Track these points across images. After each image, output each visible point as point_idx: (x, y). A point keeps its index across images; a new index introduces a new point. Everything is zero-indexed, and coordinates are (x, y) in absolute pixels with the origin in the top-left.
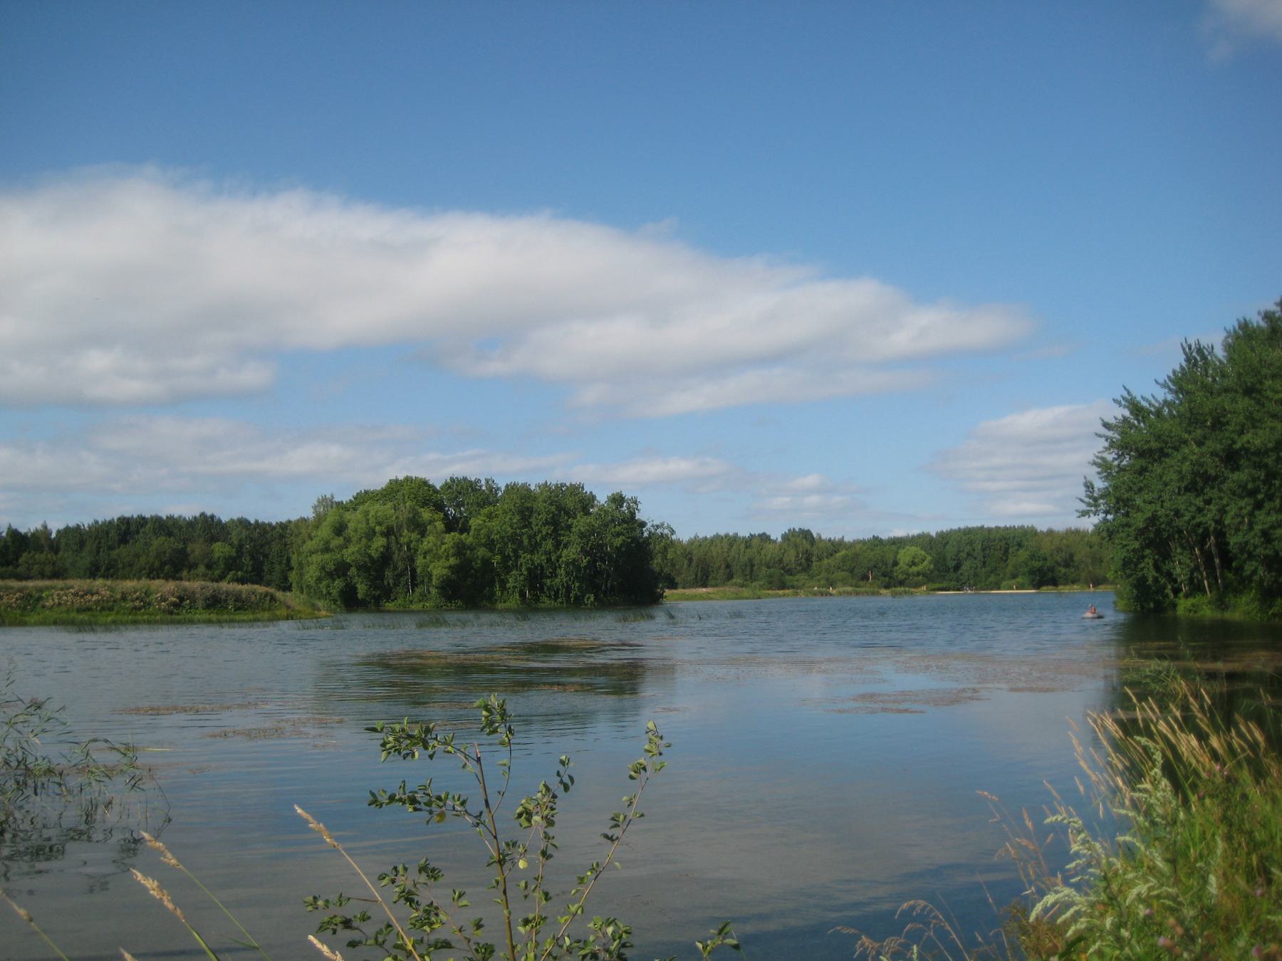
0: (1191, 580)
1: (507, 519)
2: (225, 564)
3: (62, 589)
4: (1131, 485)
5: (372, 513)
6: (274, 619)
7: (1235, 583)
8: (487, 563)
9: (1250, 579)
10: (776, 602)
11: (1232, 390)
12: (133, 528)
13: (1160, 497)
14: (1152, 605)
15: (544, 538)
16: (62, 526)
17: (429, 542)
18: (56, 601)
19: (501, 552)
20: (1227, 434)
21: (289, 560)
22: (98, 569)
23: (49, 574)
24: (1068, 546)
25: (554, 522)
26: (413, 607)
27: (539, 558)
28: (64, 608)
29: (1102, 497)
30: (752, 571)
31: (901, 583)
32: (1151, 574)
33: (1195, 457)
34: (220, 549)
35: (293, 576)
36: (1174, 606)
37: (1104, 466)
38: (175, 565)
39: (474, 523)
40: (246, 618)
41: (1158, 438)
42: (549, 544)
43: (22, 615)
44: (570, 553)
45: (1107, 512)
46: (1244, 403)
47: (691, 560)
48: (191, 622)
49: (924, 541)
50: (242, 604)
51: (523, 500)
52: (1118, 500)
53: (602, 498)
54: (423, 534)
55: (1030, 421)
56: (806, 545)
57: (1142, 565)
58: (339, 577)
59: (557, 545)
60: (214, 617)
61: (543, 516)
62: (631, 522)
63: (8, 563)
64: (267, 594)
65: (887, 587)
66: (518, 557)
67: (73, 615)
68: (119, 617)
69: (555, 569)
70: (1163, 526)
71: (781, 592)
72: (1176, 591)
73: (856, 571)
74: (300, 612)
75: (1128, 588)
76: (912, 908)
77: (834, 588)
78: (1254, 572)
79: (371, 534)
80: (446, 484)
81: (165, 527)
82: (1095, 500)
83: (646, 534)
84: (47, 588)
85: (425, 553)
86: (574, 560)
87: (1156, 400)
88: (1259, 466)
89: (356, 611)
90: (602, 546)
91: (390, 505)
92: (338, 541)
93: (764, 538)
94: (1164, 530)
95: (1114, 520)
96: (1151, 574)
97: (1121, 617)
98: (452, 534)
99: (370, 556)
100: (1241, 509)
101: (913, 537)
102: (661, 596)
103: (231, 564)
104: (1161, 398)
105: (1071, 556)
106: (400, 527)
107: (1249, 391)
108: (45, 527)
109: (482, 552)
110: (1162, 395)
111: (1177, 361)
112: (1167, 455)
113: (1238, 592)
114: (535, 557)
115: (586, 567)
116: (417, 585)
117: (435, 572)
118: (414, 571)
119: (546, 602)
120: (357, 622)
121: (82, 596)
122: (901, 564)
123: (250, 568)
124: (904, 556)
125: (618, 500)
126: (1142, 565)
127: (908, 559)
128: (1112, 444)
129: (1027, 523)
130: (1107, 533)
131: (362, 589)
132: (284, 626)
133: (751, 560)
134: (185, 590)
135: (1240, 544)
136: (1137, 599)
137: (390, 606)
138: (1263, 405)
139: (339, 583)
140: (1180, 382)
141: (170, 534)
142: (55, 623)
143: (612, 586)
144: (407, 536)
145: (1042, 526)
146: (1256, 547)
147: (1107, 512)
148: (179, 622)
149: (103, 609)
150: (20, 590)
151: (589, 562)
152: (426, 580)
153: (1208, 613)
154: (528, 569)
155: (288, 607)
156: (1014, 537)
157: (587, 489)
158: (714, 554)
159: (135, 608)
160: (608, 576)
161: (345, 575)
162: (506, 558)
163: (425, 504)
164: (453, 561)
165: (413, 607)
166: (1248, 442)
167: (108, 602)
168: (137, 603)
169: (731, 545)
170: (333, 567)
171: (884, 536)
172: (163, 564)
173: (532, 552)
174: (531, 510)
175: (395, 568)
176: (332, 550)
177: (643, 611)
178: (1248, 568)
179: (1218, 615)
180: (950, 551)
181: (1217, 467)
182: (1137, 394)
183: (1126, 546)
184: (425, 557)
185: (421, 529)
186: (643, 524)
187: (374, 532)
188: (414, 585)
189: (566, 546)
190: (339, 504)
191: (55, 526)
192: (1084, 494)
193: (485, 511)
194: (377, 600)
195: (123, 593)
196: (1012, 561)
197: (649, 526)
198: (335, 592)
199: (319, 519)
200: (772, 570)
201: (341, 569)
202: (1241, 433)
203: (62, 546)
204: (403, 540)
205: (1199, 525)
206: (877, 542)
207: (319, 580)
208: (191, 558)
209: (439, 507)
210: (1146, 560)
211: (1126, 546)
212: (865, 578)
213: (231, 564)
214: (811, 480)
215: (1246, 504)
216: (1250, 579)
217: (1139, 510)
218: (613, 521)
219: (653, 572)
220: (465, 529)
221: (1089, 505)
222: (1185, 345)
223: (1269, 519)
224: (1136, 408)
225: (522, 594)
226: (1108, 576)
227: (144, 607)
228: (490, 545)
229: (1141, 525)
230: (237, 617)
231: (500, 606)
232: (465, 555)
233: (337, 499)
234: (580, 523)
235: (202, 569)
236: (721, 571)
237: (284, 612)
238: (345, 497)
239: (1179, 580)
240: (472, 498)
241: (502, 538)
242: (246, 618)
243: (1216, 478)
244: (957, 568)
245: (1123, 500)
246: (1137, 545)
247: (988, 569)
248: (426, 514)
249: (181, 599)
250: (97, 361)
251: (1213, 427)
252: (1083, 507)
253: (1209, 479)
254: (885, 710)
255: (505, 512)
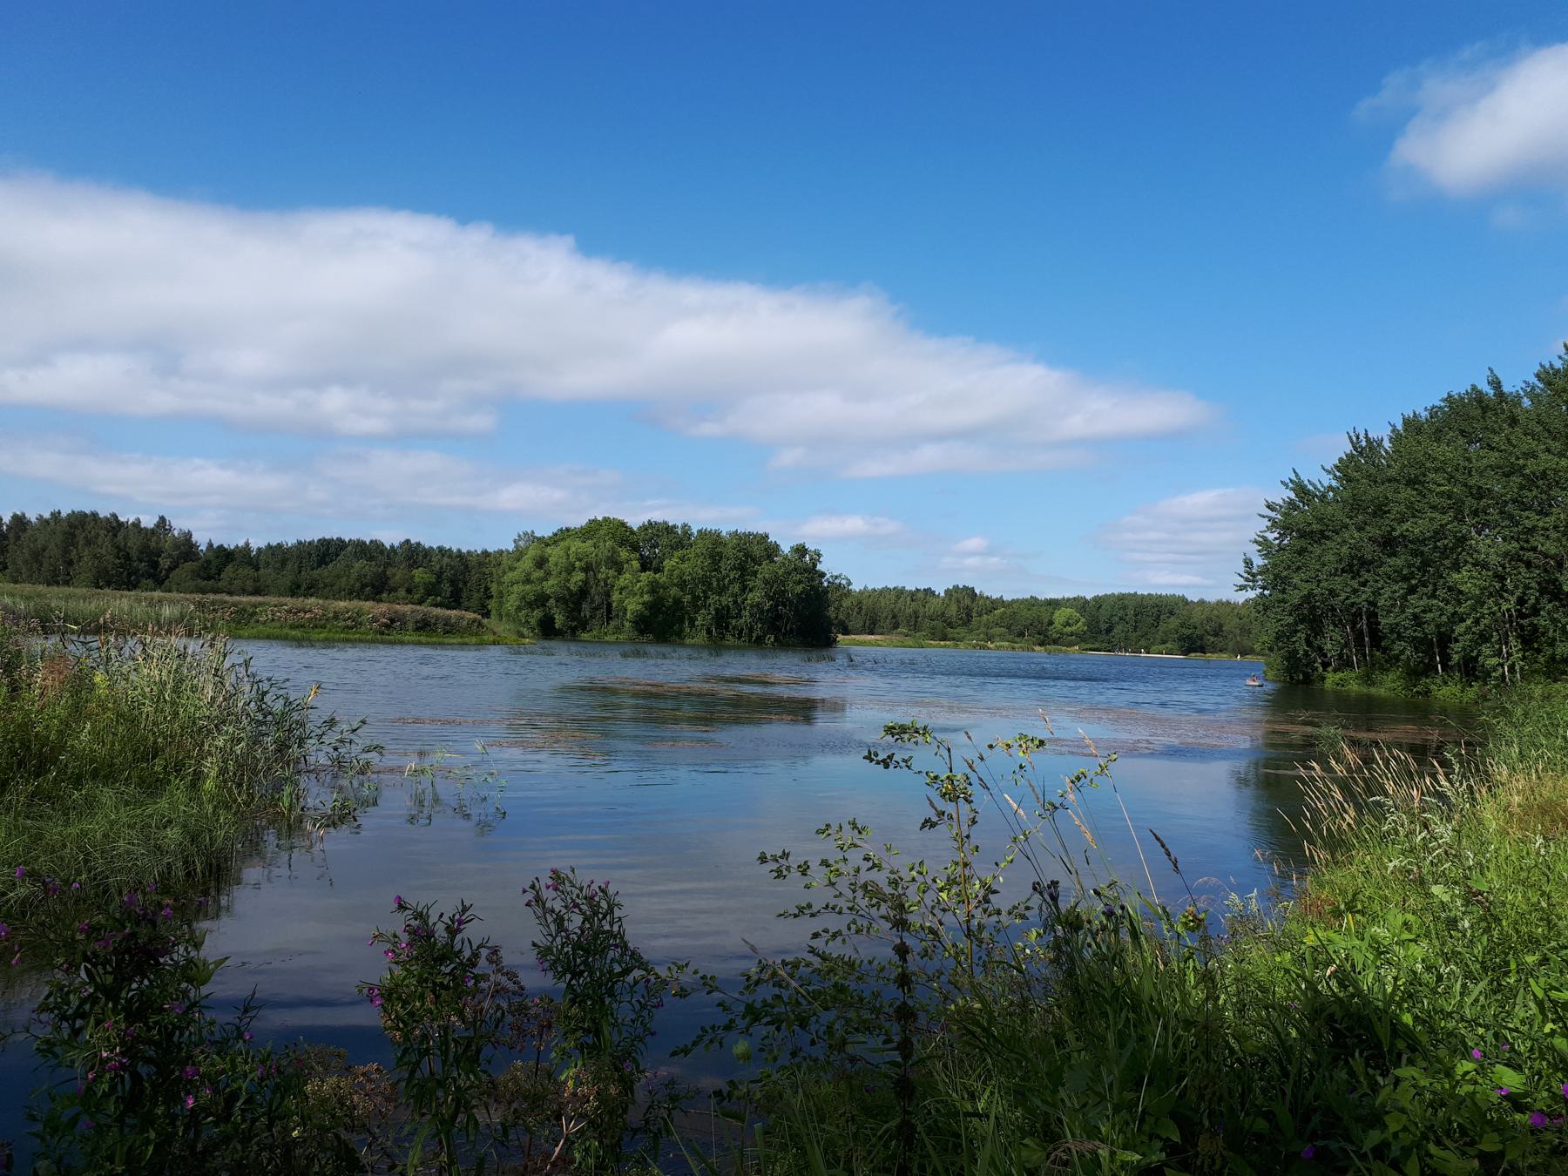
0: (1340, 656)
1: (699, 563)
2: (425, 589)
3: (275, 606)
4: (1289, 563)
5: (573, 549)
6: (481, 644)
7: (1383, 661)
8: (678, 601)
9: (1397, 658)
10: (938, 652)
11: (1395, 480)
12: (332, 550)
13: (1317, 576)
14: (1301, 677)
15: (731, 582)
16: (263, 545)
17: (625, 579)
18: (270, 616)
19: (692, 593)
20: (1387, 522)
21: (487, 589)
22: (299, 587)
23: (251, 589)
24: (1218, 617)
25: (742, 568)
26: (607, 638)
27: (726, 600)
28: (277, 624)
29: (1260, 573)
30: (916, 621)
31: (1055, 642)
32: (1302, 648)
33: (1353, 541)
34: (419, 574)
35: (492, 604)
36: (1323, 679)
37: (1263, 543)
38: (377, 588)
39: (668, 564)
40: (454, 641)
41: (1320, 520)
42: (736, 588)
43: (236, 629)
44: (755, 597)
45: (1264, 588)
46: (1406, 493)
47: (860, 608)
48: (402, 643)
49: (1080, 604)
50: (450, 629)
51: (714, 544)
52: (1276, 576)
53: (786, 548)
54: (620, 571)
55: (1200, 500)
56: (968, 601)
57: (1294, 639)
58: (538, 607)
59: (744, 589)
60: (423, 639)
61: (732, 562)
62: (812, 573)
63: (209, 578)
64: (474, 621)
65: (1041, 644)
66: (707, 598)
67: (286, 630)
68: (331, 635)
69: (741, 611)
70: (1318, 604)
71: (942, 643)
72: (1325, 665)
73: (1013, 628)
74: (506, 638)
75: (1279, 660)
76: (1206, 882)
77: (992, 643)
78: (1402, 652)
79: (570, 569)
80: (644, 525)
81: (369, 551)
82: (1254, 575)
83: (826, 584)
84: (261, 604)
85: (622, 589)
86: (758, 604)
87: (1322, 486)
88: (1415, 553)
89: (552, 639)
90: (784, 592)
91: (589, 543)
92: (539, 574)
93: (929, 592)
94: (1318, 607)
95: (1270, 595)
96: (1302, 648)
97: (1269, 687)
98: (648, 573)
99: (568, 589)
100: (1395, 592)
101: (1069, 600)
102: (835, 640)
103: (431, 590)
104: (1326, 484)
105: (1221, 626)
106: (599, 564)
107: (1411, 483)
108: (247, 544)
109: (674, 591)
110: (1328, 480)
111: (1343, 448)
112: (1328, 538)
113: (1384, 670)
114: (723, 599)
115: (768, 611)
116: (611, 618)
117: (629, 607)
118: (609, 605)
119: (730, 640)
120: (562, 652)
121: (295, 613)
122: (1056, 624)
123: (448, 595)
124: (1060, 616)
125: (801, 550)
126: (1294, 639)
127: (1063, 619)
128: (1274, 523)
129: (1179, 593)
130: (1262, 606)
131: (559, 620)
132: (495, 651)
133: (915, 612)
134: (396, 612)
135: (1391, 625)
136: (1288, 670)
137: (585, 636)
138: (1424, 496)
139: (538, 613)
140: (1346, 469)
141: (371, 558)
142: (268, 637)
143: (791, 629)
144: (604, 572)
145: (1193, 597)
146: (1406, 629)
147: (1264, 588)
148: (392, 643)
149: (316, 626)
150: (234, 604)
151: (771, 605)
152: (621, 614)
153: (1354, 687)
154: (716, 609)
155: (495, 633)
156: (1166, 606)
157: (772, 539)
158: (883, 604)
159: (347, 627)
160: (788, 619)
161: (543, 605)
162: (696, 598)
163: (621, 544)
164: (646, 598)
165: (607, 638)
166: (1407, 530)
167: (320, 620)
168: (349, 623)
169: (898, 597)
170: (533, 598)
171: (1041, 597)
172: (364, 586)
173: (720, 594)
174: (720, 555)
175: (593, 601)
176: (532, 582)
177: (825, 653)
178: (1398, 647)
179: (1364, 690)
180: (1104, 615)
181: (1374, 551)
182: (1304, 478)
183: (1280, 620)
184: (621, 593)
185: (619, 567)
186: (823, 575)
187: (574, 568)
188: (609, 618)
189: (751, 591)
190: (541, 540)
191: (257, 543)
192: (1243, 569)
193: (680, 553)
194: (573, 630)
195: (335, 612)
196: (1163, 627)
197: (828, 576)
198: (533, 621)
199: (519, 554)
200: (934, 623)
201: (541, 600)
202: (1402, 520)
203: (262, 564)
204: (600, 576)
205: (1353, 604)
206: (1033, 603)
207: (519, 609)
208: (391, 583)
209: (635, 548)
210: (1299, 635)
211: (1280, 620)
212: (1021, 634)
213: (431, 590)
214: (974, 543)
215: (1400, 588)
216: (1397, 658)
217: (1295, 587)
218: (795, 570)
219: (829, 617)
220: (658, 570)
221: (1247, 580)
222: (1352, 434)
223: (1421, 603)
224: (1300, 489)
225: (709, 632)
226: (1255, 646)
227: (356, 626)
228: (682, 585)
229: (1296, 601)
230: (445, 640)
231: (688, 641)
232: (657, 593)
233: (537, 534)
234: (765, 570)
235: (402, 593)
236: (888, 621)
237: (492, 638)
238: (546, 531)
239: (1329, 655)
240: (664, 541)
241: (693, 579)
242: (454, 641)
243: (1371, 562)
244: (1109, 631)
245: (1281, 578)
246: (1291, 620)
247: (1139, 633)
248: (624, 554)
249: (392, 621)
250: (334, 401)
251: (1374, 514)
252: (1242, 582)
253: (1364, 563)
254: (1072, 753)
255: (697, 556)
